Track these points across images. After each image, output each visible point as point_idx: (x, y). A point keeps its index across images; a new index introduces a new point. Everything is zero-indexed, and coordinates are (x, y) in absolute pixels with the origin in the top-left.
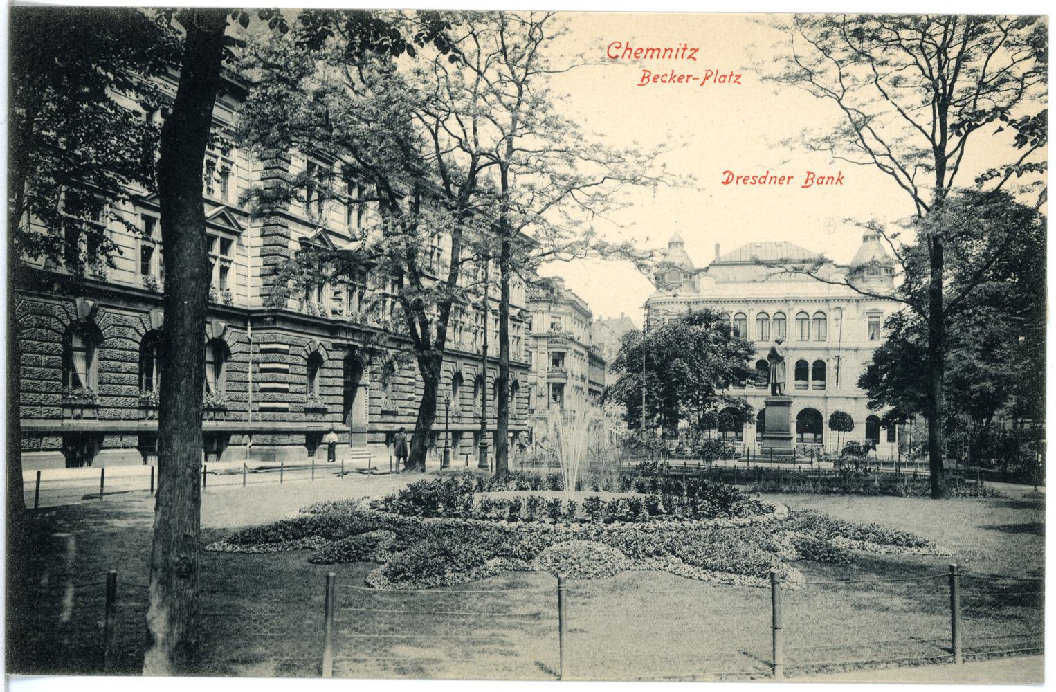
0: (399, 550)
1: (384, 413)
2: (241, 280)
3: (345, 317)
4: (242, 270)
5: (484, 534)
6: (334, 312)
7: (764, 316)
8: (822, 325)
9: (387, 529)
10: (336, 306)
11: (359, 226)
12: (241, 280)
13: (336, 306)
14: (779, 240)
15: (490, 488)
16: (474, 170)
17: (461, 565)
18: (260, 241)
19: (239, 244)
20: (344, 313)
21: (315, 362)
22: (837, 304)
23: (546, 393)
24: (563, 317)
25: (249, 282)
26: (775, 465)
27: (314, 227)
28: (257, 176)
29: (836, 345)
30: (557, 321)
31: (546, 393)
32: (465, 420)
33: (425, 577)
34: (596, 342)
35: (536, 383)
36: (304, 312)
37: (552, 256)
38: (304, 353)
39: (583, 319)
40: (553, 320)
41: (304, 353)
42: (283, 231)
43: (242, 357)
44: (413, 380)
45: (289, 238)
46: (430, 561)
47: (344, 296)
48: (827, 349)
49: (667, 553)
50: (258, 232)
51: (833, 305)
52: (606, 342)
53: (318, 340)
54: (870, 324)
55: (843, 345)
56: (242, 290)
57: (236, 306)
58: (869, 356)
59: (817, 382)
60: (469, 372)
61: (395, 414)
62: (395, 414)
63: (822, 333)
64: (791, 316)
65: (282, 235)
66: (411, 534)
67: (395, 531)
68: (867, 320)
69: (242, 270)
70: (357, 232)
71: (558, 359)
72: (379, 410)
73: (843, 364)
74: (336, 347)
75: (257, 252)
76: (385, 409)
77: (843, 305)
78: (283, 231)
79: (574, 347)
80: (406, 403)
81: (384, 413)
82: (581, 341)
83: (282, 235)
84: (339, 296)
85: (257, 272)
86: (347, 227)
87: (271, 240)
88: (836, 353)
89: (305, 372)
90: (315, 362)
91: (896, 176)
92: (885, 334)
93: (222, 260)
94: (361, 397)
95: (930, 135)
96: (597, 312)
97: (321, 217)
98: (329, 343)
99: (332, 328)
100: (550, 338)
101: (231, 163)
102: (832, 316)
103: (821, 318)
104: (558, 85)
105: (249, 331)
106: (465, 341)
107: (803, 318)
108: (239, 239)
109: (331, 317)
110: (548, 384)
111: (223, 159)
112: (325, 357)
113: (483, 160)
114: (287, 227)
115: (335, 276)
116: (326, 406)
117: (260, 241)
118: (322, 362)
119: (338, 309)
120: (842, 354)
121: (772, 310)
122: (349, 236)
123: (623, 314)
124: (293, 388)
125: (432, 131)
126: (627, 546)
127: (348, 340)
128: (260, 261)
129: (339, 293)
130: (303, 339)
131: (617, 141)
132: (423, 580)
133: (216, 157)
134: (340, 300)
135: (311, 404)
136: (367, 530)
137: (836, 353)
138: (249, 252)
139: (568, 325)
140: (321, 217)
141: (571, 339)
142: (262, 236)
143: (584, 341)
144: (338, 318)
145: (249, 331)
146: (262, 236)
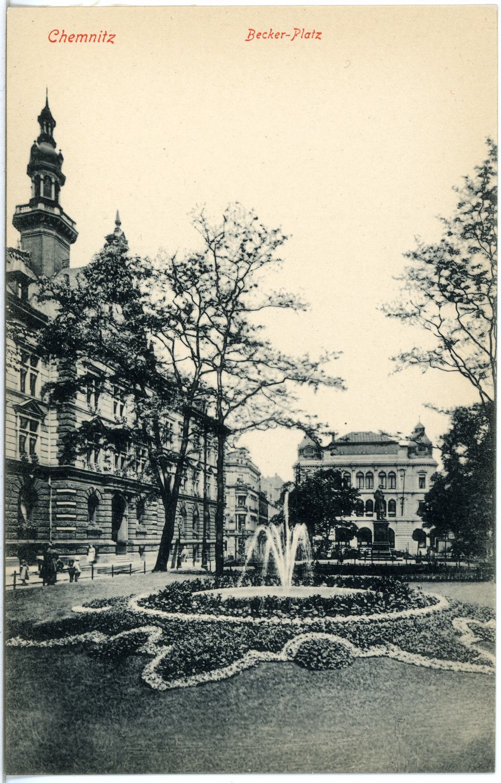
0: (167, 645)
1: (137, 533)
2: (44, 448)
3: (111, 472)
4: (44, 441)
5: (237, 630)
6: (105, 469)
7: (360, 475)
8: (393, 480)
9: (154, 625)
10: (106, 465)
11: (121, 415)
12: (44, 448)
13: (106, 465)
14: (367, 430)
15: (223, 584)
16: (199, 374)
17: (224, 660)
18: (57, 423)
19: (43, 425)
20: (112, 470)
21: (93, 502)
22: (402, 468)
23: (234, 520)
24: (244, 475)
25: (49, 449)
26: (383, 562)
27: (94, 414)
28: (56, 374)
29: (401, 491)
30: (241, 477)
31: (234, 520)
32: (188, 537)
33: (195, 674)
34: (263, 490)
35: (229, 515)
36: (86, 469)
37: (253, 427)
38: (86, 495)
39: (255, 476)
40: (238, 477)
41: (86, 495)
42: (72, 416)
43: (46, 497)
44: (156, 513)
45: (76, 421)
46: (197, 658)
47: (112, 459)
48: (396, 493)
49: (386, 642)
50: (55, 416)
51: (399, 468)
52: (268, 491)
53: (95, 487)
54: (420, 478)
55: (406, 491)
56: (44, 454)
57: (40, 464)
58: (422, 497)
59: (391, 513)
60: (189, 506)
61: (145, 533)
62: (145, 533)
63: (394, 485)
64: (376, 475)
65: (71, 419)
66: (175, 629)
67: (161, 627)
68: (418, 476)
69: (44, 441)
70: (120, 419)
71: (242, 499)
72: (134, 531)
73: (406, 502)
74: (107, 491)
75: (55, 430)
76: (138, 530)
77: (404, 468)
78: (72, 416)
79: (250, 492)
80: (152, 527)
81: (137, 533)
82: (255, 489)
83: (71, 419)
84: (108, 459)
85: (55, 443)
86: (113, 415)
87: (65, 422)
88: (401, 495)
89: (87, 507)
90: (93, 502)
91: (470, 379)
92: (429, 485)
93: (31, 434)
94: (124, 523)
95: (489, 351)
96: (265, 474)
97: (96, 409)
98: (101, 489)
99: (104, 480)
100: (237, 488)
101: (38, 372)
102: (399, 474)
103: (393, 476)
104: (251, 318)
105: (50, 481)
106: (188, 489)
107: (382, 476)
108: (43, 421)
109: (103, 472)
110: (236, 515)
111: (32, 369)
112: (100, 498)
113: (205, 367)
114: (74, 414)
115: (106, 443)
116: (101, 529)
117: (57, 423)
118: (98, 500)
119: (108, 467)
120: (405, 496)
121: (365, 471)
122: (115, 421)
123: (276, 474)
124: (79, 517)
125: (169, 350)
126: (354, 636)
127: (114, 487)
128: (56, 436)
129: (109, 457)
130: (87, 486)
131: (295, 354)
132: (193, 677)
133: (27, 367)
134: (109, 462)
135: (91, 528)
136: (138, 625)
137: (401, 495)
138: (49, 430)
139: (247, 479)
140: (96, 409)
141: (250, 489)
142: (58, 419)
143: (256, 489)
144: (108, 473)
145: (50, 481)
146: (58, 419)
